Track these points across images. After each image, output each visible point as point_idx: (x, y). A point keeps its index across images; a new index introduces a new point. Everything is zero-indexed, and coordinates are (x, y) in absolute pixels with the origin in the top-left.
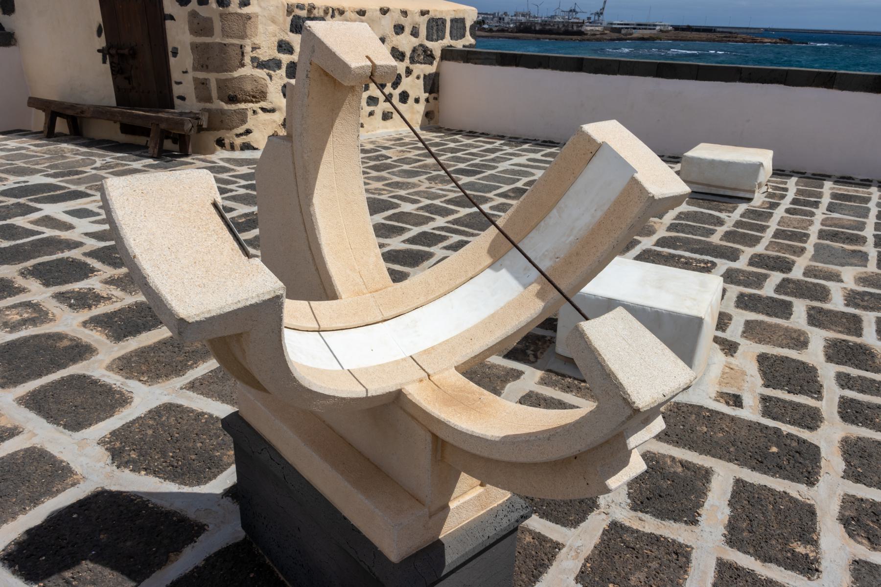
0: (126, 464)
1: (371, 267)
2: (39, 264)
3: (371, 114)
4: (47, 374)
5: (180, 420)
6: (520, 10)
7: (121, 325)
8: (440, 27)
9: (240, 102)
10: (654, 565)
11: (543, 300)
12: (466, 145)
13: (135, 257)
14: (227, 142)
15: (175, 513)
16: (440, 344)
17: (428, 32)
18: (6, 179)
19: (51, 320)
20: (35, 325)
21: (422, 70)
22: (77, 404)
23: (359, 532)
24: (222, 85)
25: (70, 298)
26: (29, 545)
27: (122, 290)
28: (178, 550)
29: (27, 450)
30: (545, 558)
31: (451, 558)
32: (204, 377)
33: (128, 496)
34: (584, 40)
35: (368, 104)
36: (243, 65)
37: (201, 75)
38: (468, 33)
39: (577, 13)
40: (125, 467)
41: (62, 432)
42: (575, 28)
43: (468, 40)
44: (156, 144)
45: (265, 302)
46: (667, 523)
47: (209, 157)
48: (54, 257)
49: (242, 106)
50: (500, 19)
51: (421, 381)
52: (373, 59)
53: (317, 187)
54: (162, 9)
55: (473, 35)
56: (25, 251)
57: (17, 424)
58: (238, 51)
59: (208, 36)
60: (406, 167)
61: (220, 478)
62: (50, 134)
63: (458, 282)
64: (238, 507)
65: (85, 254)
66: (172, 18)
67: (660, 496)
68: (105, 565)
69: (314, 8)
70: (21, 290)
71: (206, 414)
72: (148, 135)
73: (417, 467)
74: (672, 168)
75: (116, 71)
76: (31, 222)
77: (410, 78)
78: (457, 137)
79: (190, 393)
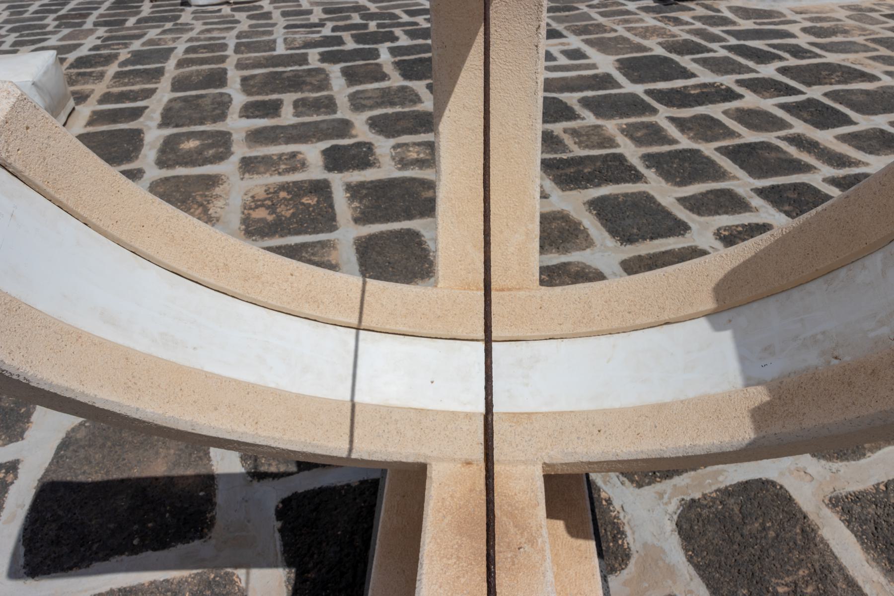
11: (758, 428)
16: (545, 415)
20: (421, 168)
51: (469, 463)
63: (638, 322)
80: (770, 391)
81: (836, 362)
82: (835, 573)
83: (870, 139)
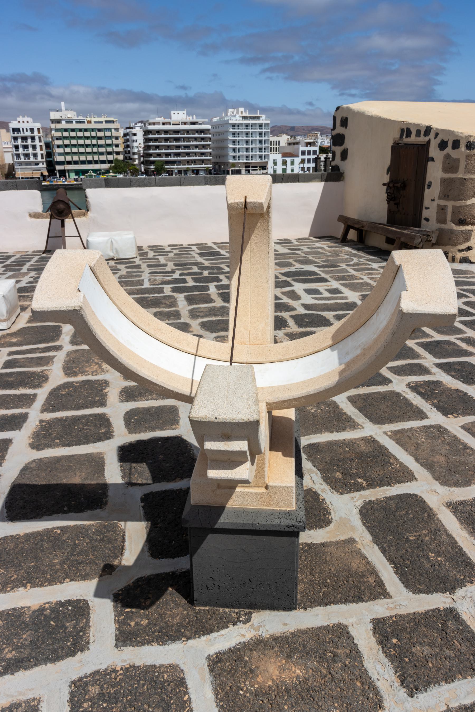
9: (468, 224)
24: (456, 210)
31: (224, 520)
37: (443, 203)
54: (428, 153)
59: (453, 173)
62: (344, 240)
66: (433, 160)
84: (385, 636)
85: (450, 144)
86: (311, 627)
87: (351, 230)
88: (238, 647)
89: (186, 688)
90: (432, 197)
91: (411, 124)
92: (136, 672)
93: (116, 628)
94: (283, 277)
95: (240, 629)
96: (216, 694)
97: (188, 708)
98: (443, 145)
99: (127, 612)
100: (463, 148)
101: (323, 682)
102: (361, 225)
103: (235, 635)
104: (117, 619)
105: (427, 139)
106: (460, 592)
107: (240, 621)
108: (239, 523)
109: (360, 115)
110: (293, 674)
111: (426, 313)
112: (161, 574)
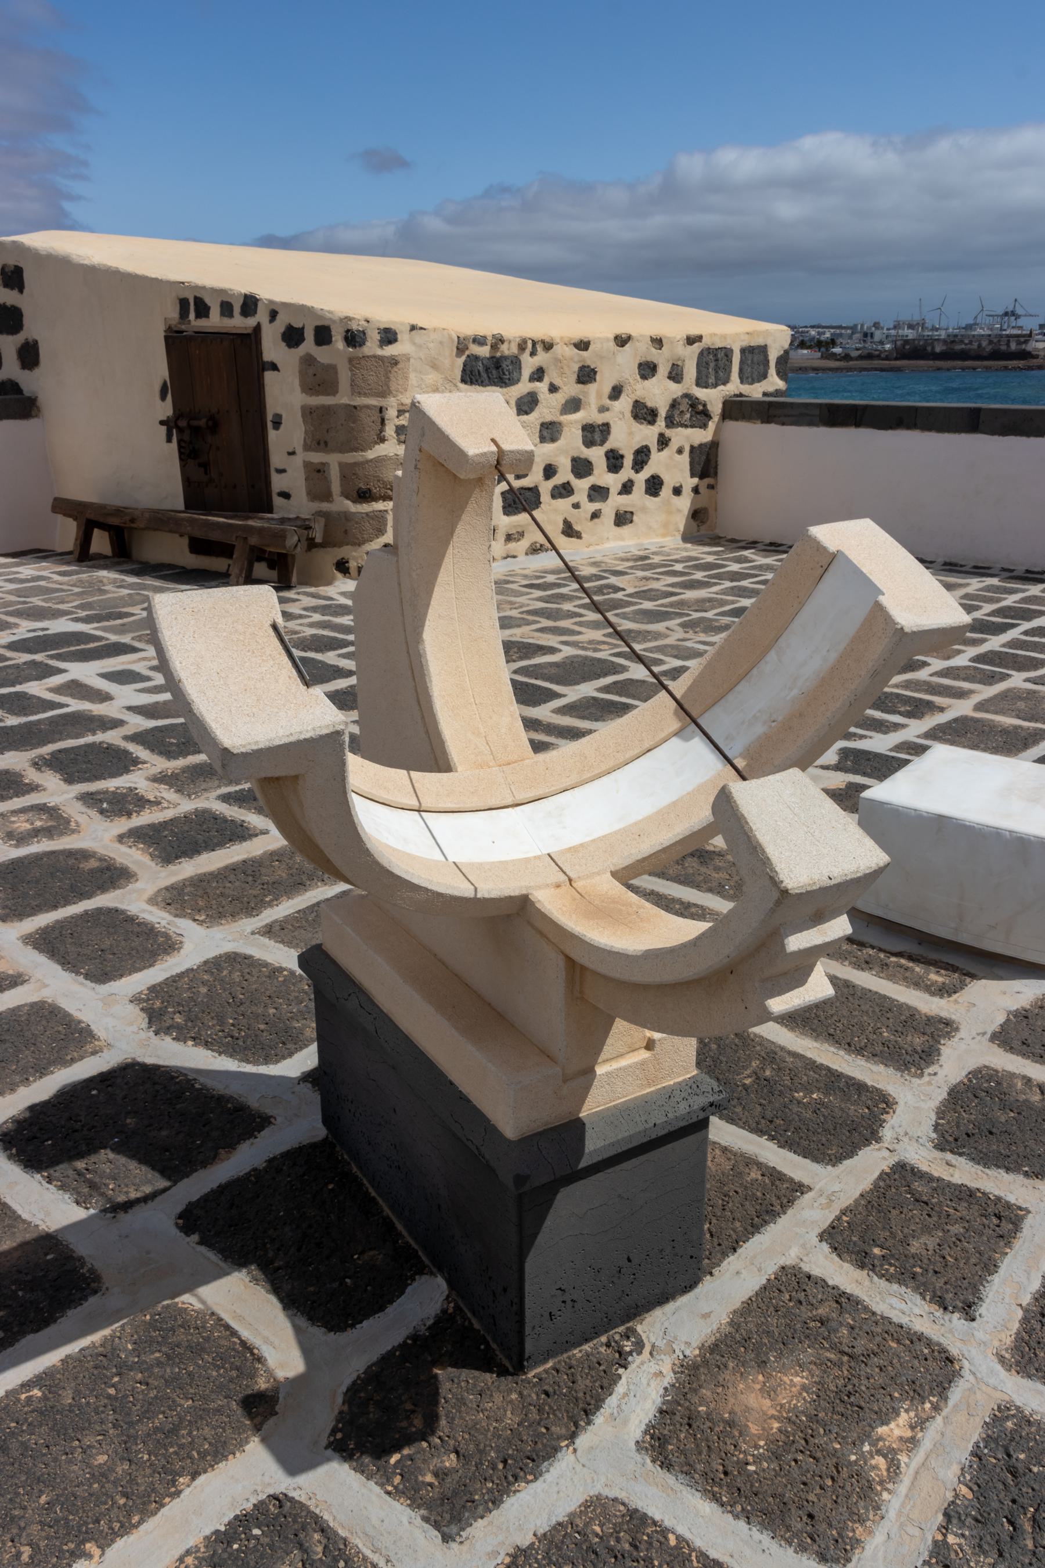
0: (167, 1031)
1: (503, 730)
2: (60, 751)
3: (595, 515)
4: (64, 906)
5: (247, 977)
6: (905, 317)
7: (172, 841)
8: (721, 364)
10: (956, 1229)
12: (760, 567)
13: (180, 681)
14: (353, 565)
15: (230, 1099)
16: (593, 841)
17: (699, 371)
18: (16, 625)
19: (73, 831)
21: (688, 438)
22: (104, 947)
23: (469, 1101)
24: (348, 472)
25: (101, 801)
26: (31, 1124)
27: (178, 791)
28: (231, 1146)
29: (33, 1005)
30: (776, 1202)
31: (595, 1145)
32: (287, 919)
33: (167, 1072)
34: (1030, 368)
35: (591, 499)
36: (382, 440)
37: (316, 457)
38: (772, 371)
39: (1018, 317)
40: (166, 1034)
41: (82, 984)
42: (1013, 346)
43: (773, 383)
44: (241, 572)
45: (321, 737)
46: (993, 1172)
47: (323, 590)
48: (81, 741)
49: (380, 506)
50: (866, 335)
51: (558, 886)
52: (500, 443)
53: (429, 617)
55: (781, 374)
56: (40, 731)
57: (21, 970)
58: (376, 417)
59: (328, 395)
60: (647, 605)
61: (298, 1056)
62: (83, 556)
63: (627, 756)
64: (319, 1097)
65: (126, 738)
66: (274, 367)
67: (991, 1133)
68: (132, 1157)
69: (502, 341)
70: (33, 788)
71: (285, 969)
72: (230, 556)
73: (546, 1007)
74: (949, 587)
75: (188, 454)
76: (51, 690)
77: (666, 452)
78: (746, 553)
79: (266, 940)
80: (744, 758)
81: (773, 724)
82: (780, 1053)
83: (588, 708)
84: (859, 1252)
85: (309, 335)
86: (747, 1297)
87: (96, 531)
88: (669, 1398)
89: (655, 1523)
90: (288, 449)
91: (204, 288)
92: (536, 1558)
93: (409, 1505)
94: (20, 654)
95: (644, 1368)
96: (715, 1498)
97: (694, 1554)
98: (293, 337)
99: (398, 1462)
100: (339, 344)
101: (846, 1372)
102: (127, 518)
103: (644, 1382)
104: (390, 1488)
105: (251, 322)
106: (887, 1133)
107: (630, 1353)
108: (623, 1139)
109: (61, 265)
110: (794, 1389)
111: (935, 627)
112: (390, 1354)
